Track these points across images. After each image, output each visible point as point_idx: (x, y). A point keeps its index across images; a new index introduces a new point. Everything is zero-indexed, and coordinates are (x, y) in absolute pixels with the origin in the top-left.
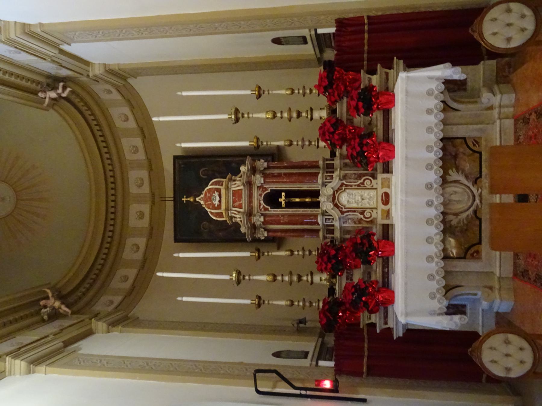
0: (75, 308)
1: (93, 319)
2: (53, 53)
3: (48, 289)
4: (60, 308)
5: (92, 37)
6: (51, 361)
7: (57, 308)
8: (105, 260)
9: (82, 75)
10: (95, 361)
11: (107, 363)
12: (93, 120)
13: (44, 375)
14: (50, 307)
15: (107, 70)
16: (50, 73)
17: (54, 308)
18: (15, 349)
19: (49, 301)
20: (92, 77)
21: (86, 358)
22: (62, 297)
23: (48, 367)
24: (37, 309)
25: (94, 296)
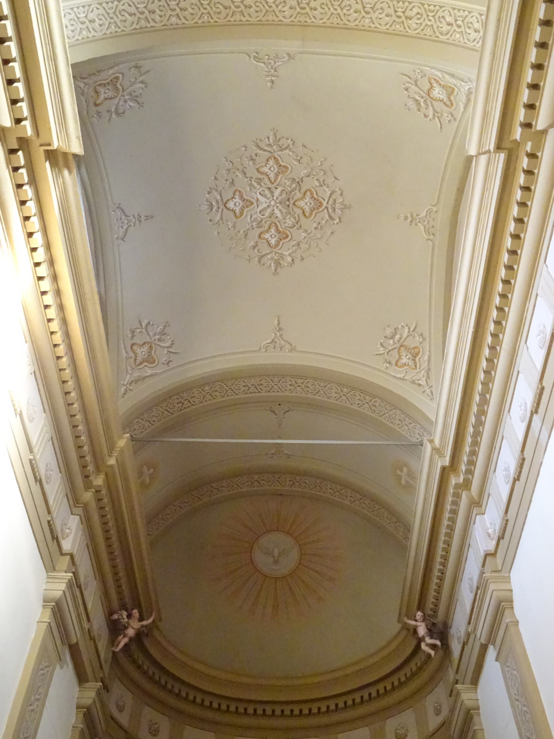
0: (123, 660)
1: (101, 684)
2: (480, 636)
3: (154, 621)
4: (124, 636)
5: (515, 694)
6: (56, 634)
7: (126, 632)
8: (186, 699)
9: (457, 672)
10: (40, 691)
11: (32, 711)
12: (393, 683)
13: (37, 620)
14: (128, 623)
15: (471, 711)
16: (451, 627)
17: (126, 628)
18: (80, 582)
19: (137, 621)
20: (456, 688)
21: (46, 678)
22: (139, 636)
23: (47, 626)
24: (128, 606)
25: (132, 681)
